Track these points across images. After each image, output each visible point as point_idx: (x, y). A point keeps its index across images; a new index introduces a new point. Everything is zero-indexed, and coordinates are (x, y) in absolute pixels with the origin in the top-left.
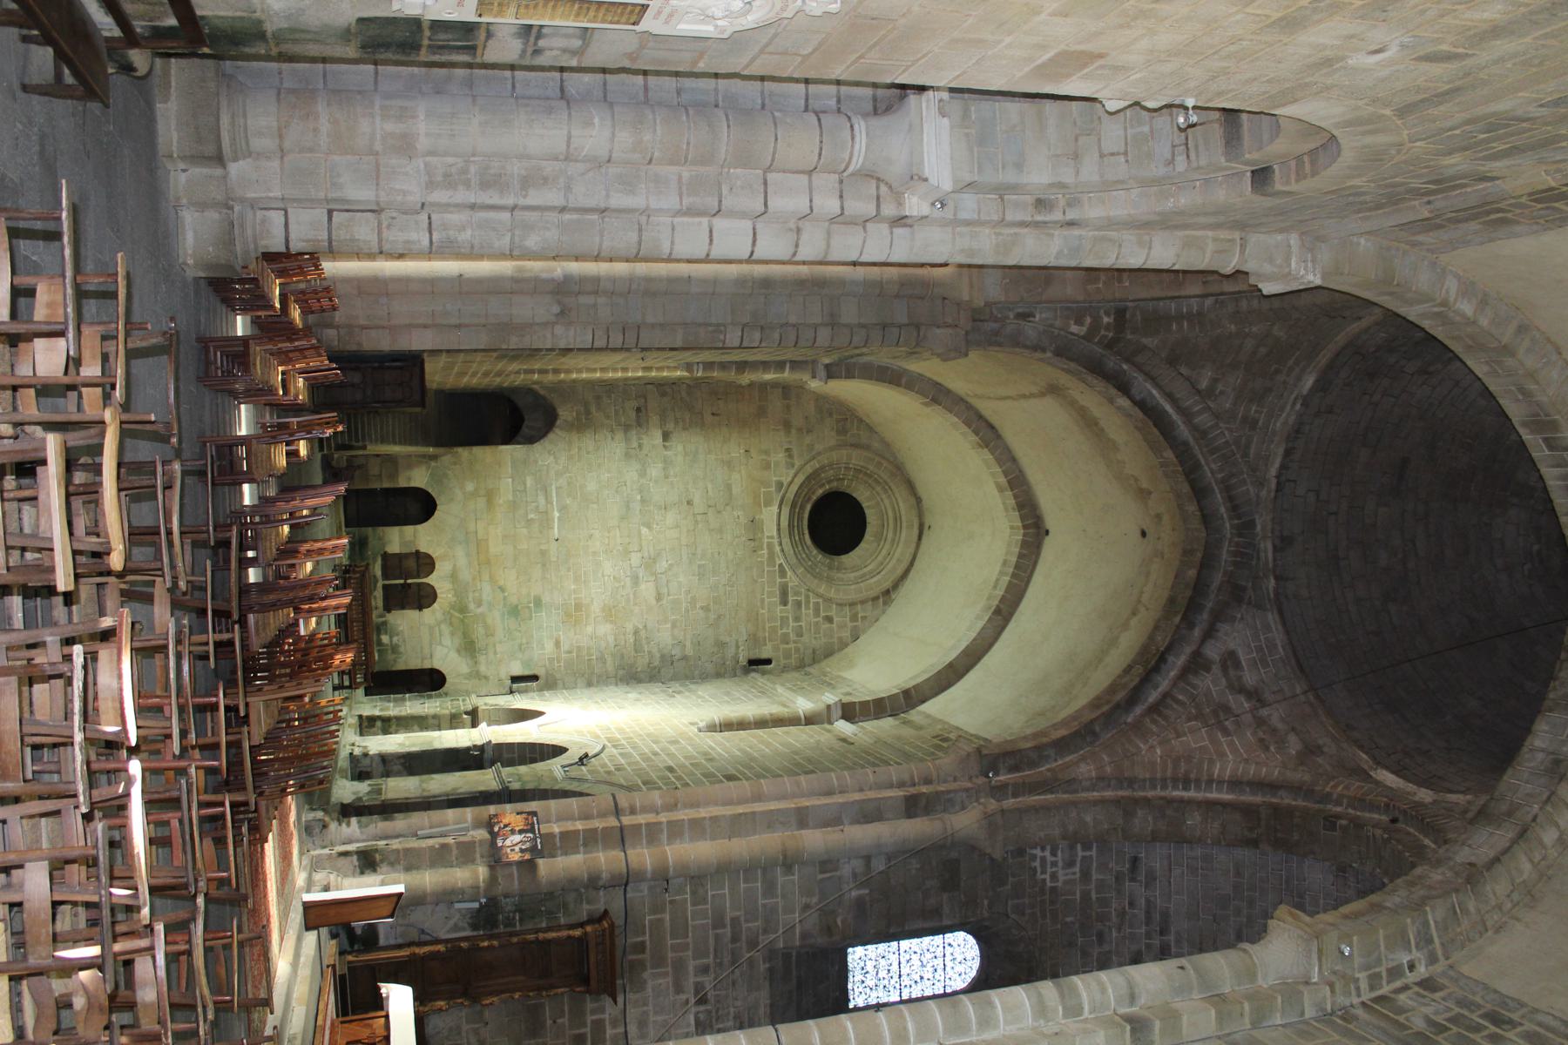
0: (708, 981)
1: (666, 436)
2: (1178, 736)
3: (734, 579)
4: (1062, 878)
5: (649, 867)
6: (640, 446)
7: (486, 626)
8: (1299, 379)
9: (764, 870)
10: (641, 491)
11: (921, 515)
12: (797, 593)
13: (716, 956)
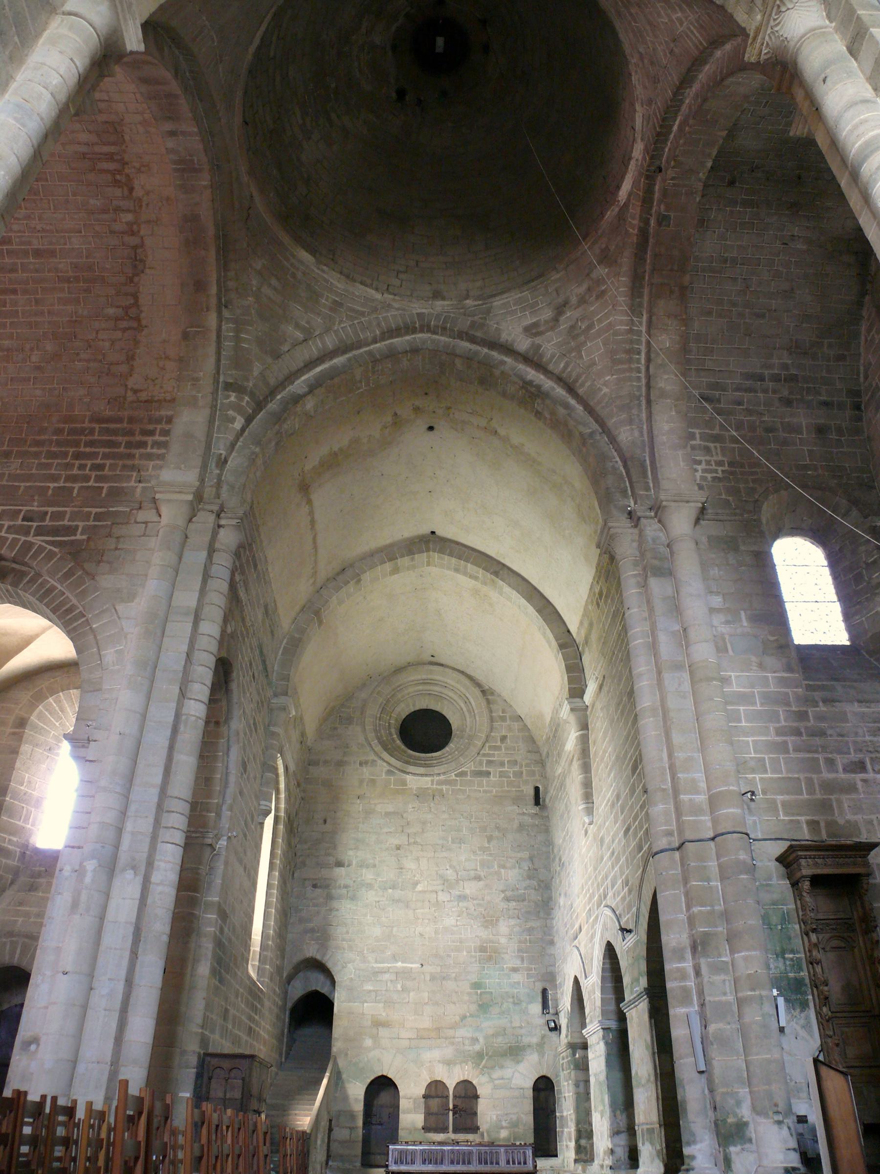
0: (840, 761)
1: (340, 864)
2: (594, 364)
3: (465, 814)
4: (720, 458)
6: (346, 887)
7: (495, 1035)
8: (301, 262)
10: (385, 889)
12: (481, 763)
13: (816, 752)
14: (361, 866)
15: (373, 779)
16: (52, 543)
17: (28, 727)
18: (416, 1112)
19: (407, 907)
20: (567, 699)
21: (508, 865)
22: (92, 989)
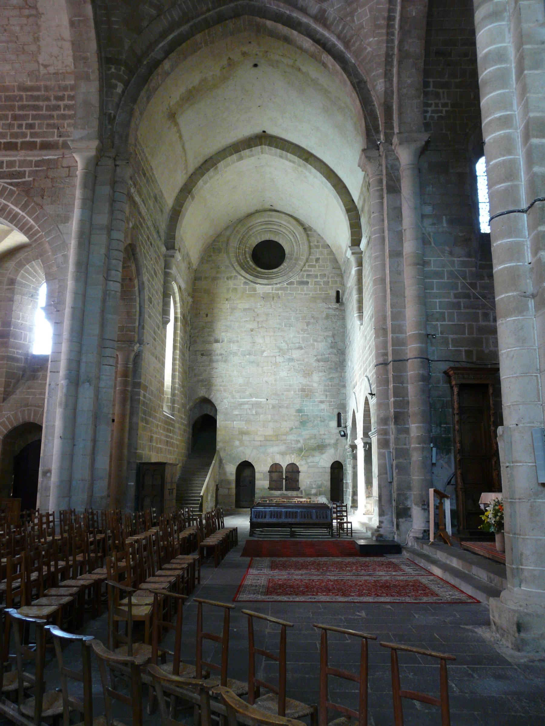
1: (217, 341)
3: (293, 309)
5: (418, 345)
6: (221, 354)
7: (310, 439)
9: (426, 278)
10: (245, 355)
11: (265, 211)
14: (230, 342)
15: (236, 288)
16: (11, 184)
17: (16, 284)
18: (265, 480)
19: (258, 366)
20: (349, 247)
21: (319, 340)
22: (74, 445)
